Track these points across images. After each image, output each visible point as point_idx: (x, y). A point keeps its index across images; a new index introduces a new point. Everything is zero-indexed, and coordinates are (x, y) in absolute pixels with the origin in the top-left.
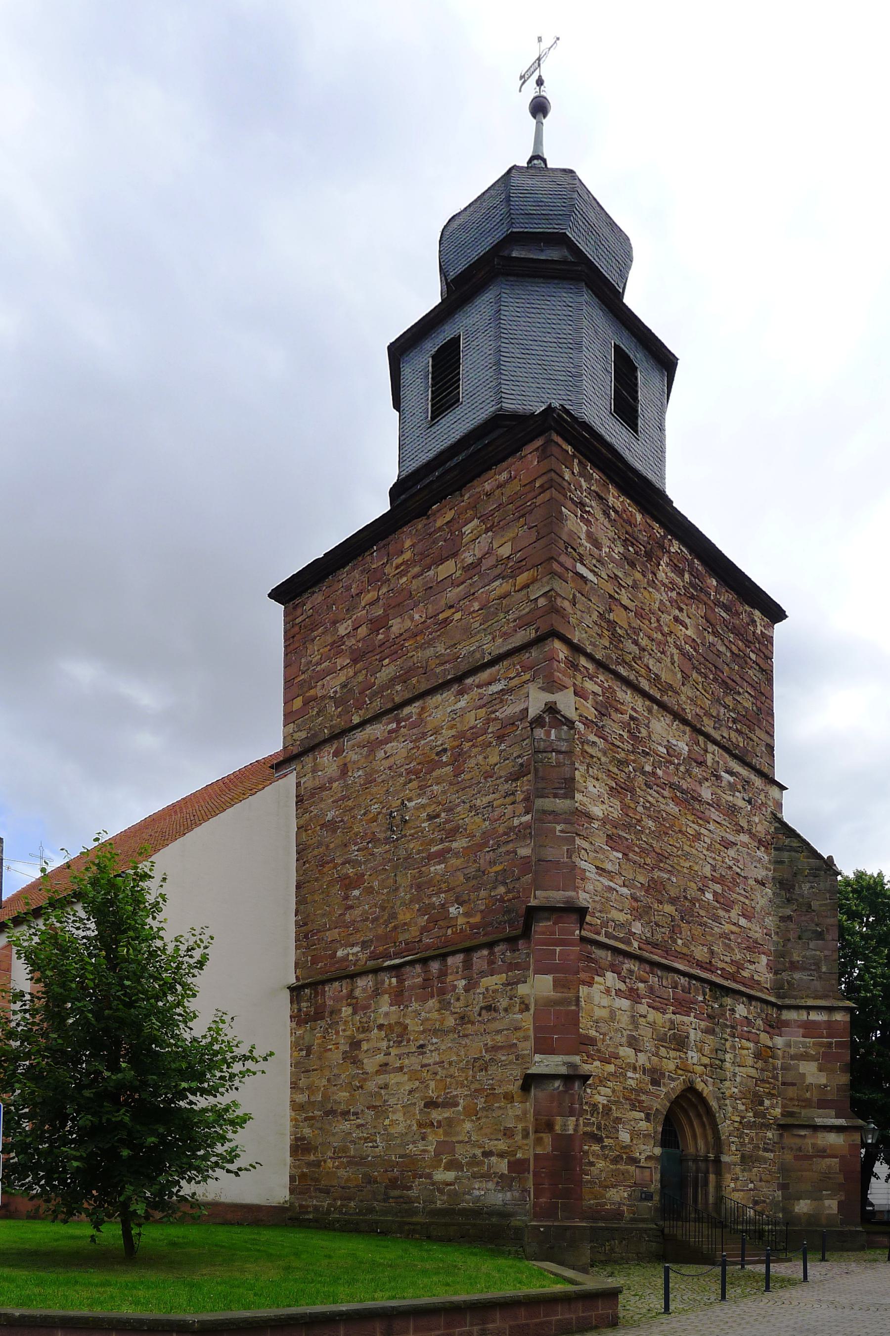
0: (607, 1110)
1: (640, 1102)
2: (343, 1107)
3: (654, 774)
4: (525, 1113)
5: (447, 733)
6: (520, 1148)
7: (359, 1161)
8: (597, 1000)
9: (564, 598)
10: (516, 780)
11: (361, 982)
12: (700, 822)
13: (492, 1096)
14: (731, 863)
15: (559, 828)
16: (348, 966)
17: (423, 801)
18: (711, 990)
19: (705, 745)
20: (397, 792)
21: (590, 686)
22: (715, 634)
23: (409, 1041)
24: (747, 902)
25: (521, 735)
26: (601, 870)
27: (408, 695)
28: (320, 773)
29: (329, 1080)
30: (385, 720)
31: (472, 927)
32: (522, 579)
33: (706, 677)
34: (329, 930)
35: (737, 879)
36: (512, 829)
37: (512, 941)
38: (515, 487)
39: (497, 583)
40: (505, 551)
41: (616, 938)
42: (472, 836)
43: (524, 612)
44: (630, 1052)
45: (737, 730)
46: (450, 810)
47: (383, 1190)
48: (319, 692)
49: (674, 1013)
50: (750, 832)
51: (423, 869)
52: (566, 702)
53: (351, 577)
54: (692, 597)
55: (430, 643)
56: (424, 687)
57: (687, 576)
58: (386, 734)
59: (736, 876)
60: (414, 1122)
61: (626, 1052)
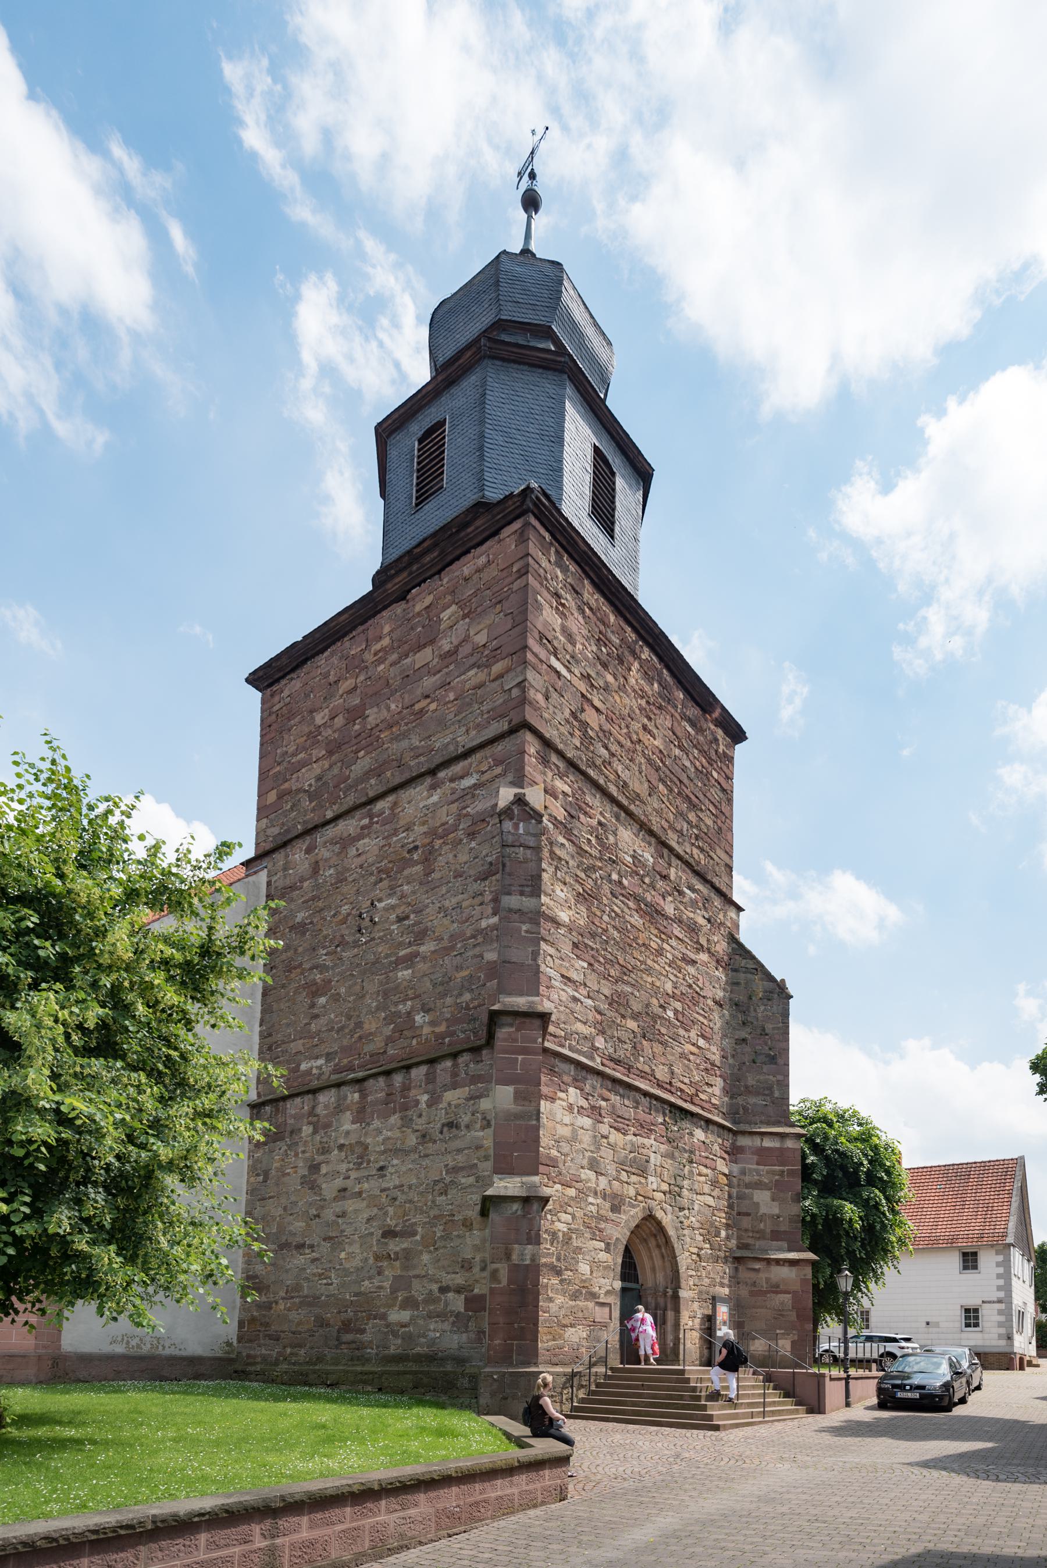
2: (299, 1239)
3: (620, 882)
5: (419, 829)
6: (477, 1281)
7: (313, 1301)
9: (537, 690)
11: (323, 1098)
12: (663, 936)
14: (691, 981)
15: (524, 928)
16: (311, 1081)
17: (392, 901)
18: (670, 1112)
19: (670, 859)
21: (561, 785)
22: (681, 747)
23: (369, 1162)
24: (706, 1022)
25: (491, 832)
27: (381, 789)
28: (291, 871)
29: (285, 1209)
30: (358, 814)
31: (440, 1037)
32: (497, 668)
33: (671, 790)
34: (294, 1041)
36: (480, 931)
37: (475, 1050)
38: (492, 572)
39: (472, 672)
40: (481, 639)
41: (579, 1052)
43: (498, 703)
44: (592, 1175)
45: (699, 847)
47: (335, 1334)
48: (292, 784)
49: (635, 1135)
50: (709, 951)
51: (391, 974)
52: (535, 797)
53: (328, 663)
55: (405, 735)
56: (397, 780)
57: (656, 685)
58: (359, 830)
59: (695, 995)
60: (371, 1255)
61: (588, 1174)
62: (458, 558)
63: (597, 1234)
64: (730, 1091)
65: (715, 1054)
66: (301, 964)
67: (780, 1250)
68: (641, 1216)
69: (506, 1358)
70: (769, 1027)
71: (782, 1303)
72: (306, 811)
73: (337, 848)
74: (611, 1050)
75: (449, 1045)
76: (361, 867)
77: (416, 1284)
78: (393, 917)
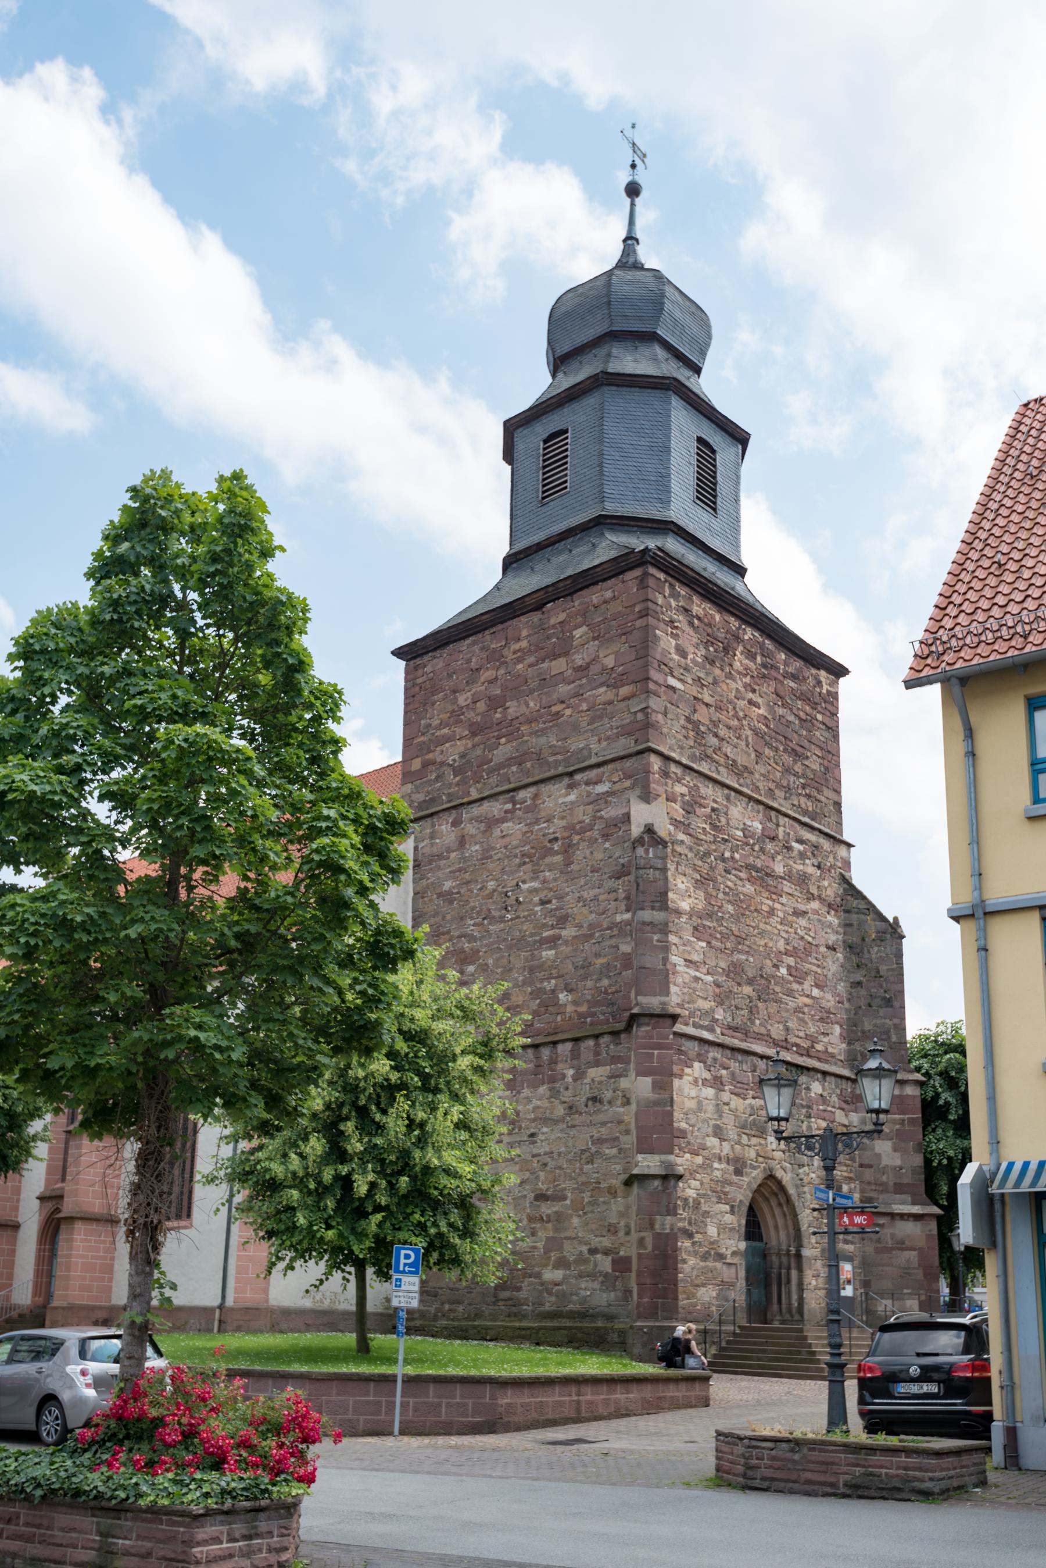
0: (697, 1204)
1: (725, 1193)
3: (733, 858)
4: (628, 1207)
8: (686, 1091)
10: (618, 878)
13: (596, 1189)
15: (655, 938)
17: (535, 884)
20: (512, 873)
23: (520, 1128)
24: (819, 971)
26: (689, 962)
31: (581, 1016)
32: (624, 691)
33: (777, 750)
35: (809, 948)
36: (616, 925)
38: (617, 607)
39: (603, 689)
40: (610, 662)
41: (701, 1027)
42: (580, 926)
46: (560, 898)
48: (436, 756)
50: (820, 897)
54: (764, 676)
55: (542, 732)
60: (524, 1217)
61: (712, 1142)
62: (587, 586)
63: (722, 1198)
64: (849, 1038)
65: (829, 1000)
66: (449, 932)
67: (903, 1203)
68: (761, 1176)
69: (653, 1315)
70: (883, 968)
71: (908, 1261)
72: (450, 784)
73: (482, 827)
74: (730, 1019)
75: (591, 1024)
76: (506, 847)
77: (567, 1246)
78: (536, 899)
